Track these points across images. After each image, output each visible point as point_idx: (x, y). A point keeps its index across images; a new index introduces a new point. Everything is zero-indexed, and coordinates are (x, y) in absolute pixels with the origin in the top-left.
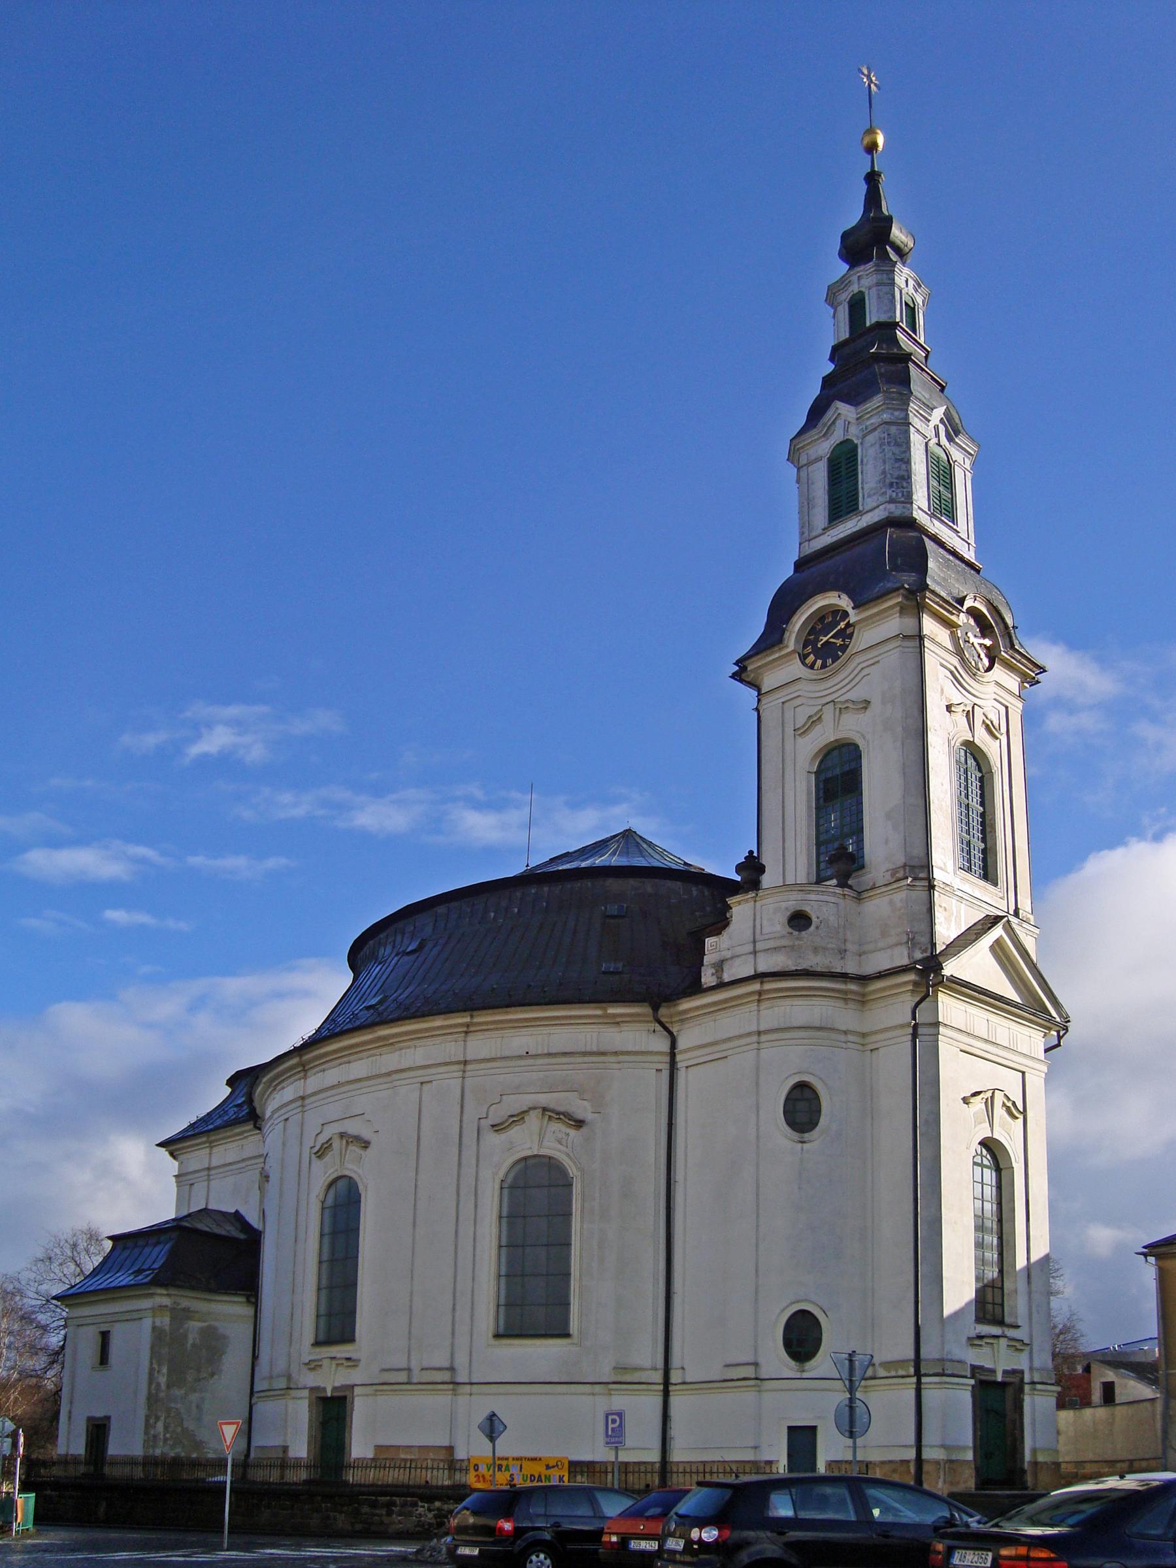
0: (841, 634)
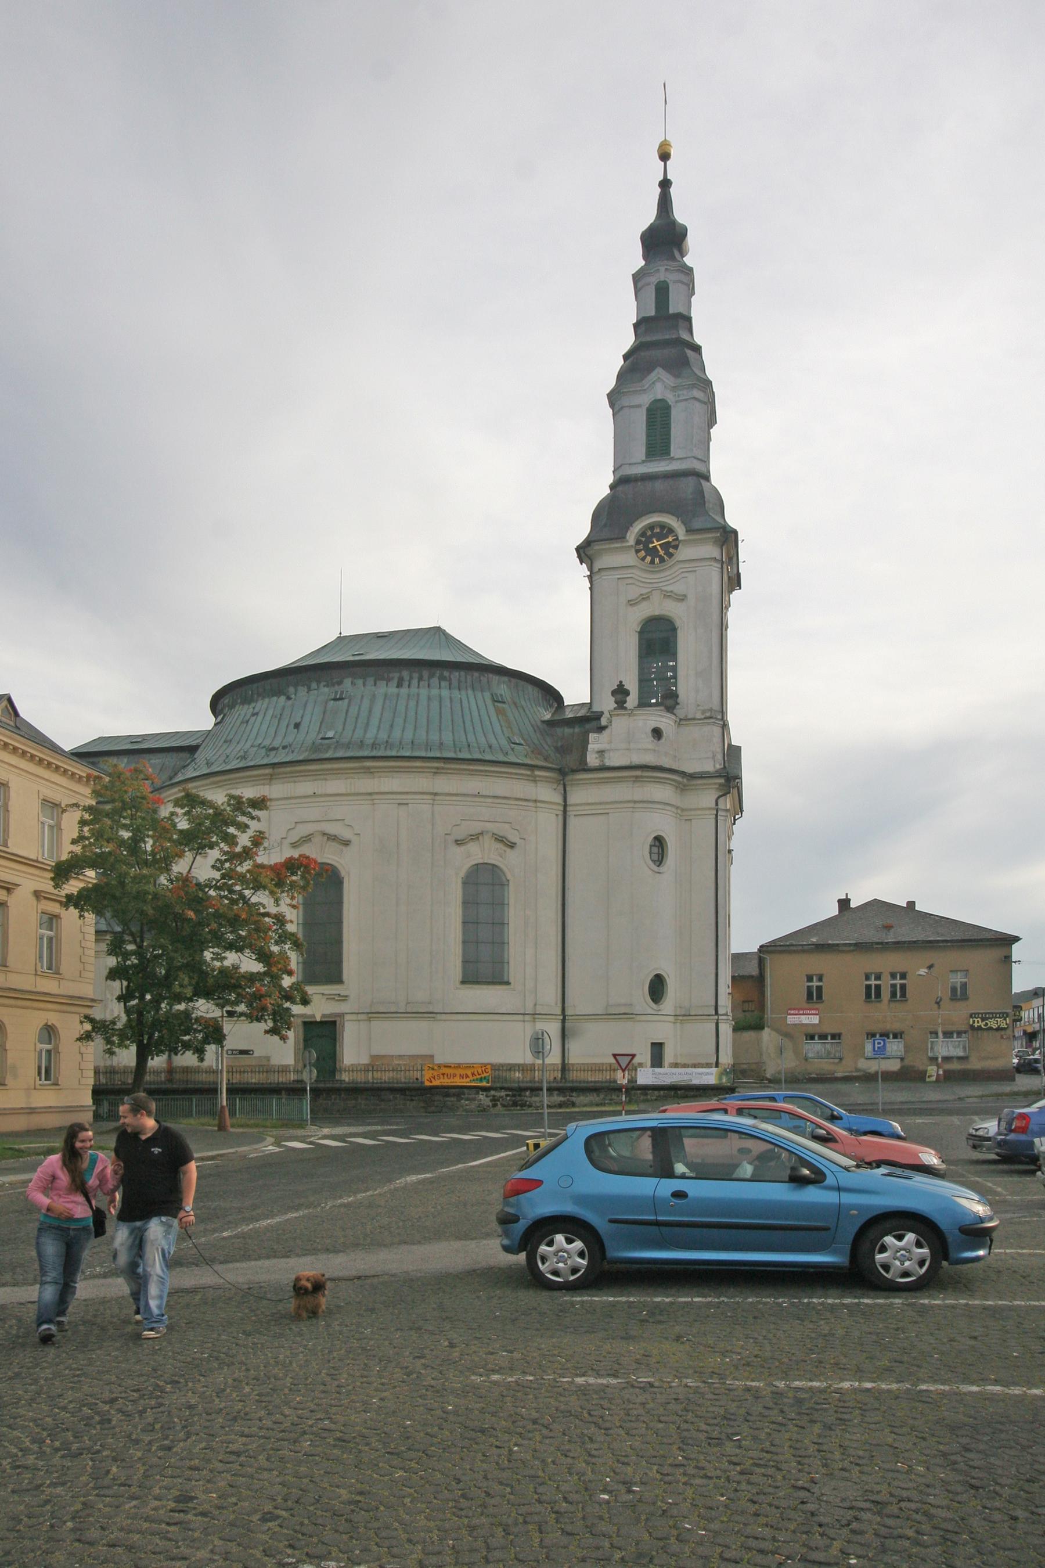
0: (666, 546)
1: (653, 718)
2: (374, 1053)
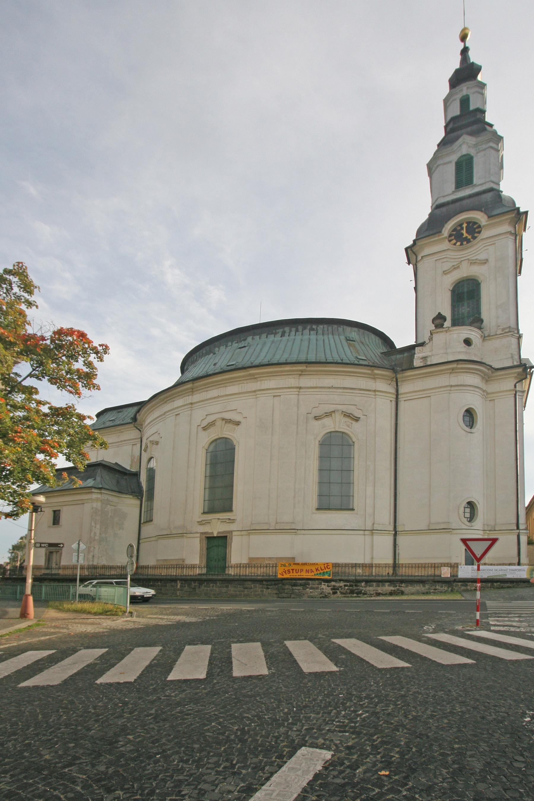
1: (465, 332)
2: (252, 555)
